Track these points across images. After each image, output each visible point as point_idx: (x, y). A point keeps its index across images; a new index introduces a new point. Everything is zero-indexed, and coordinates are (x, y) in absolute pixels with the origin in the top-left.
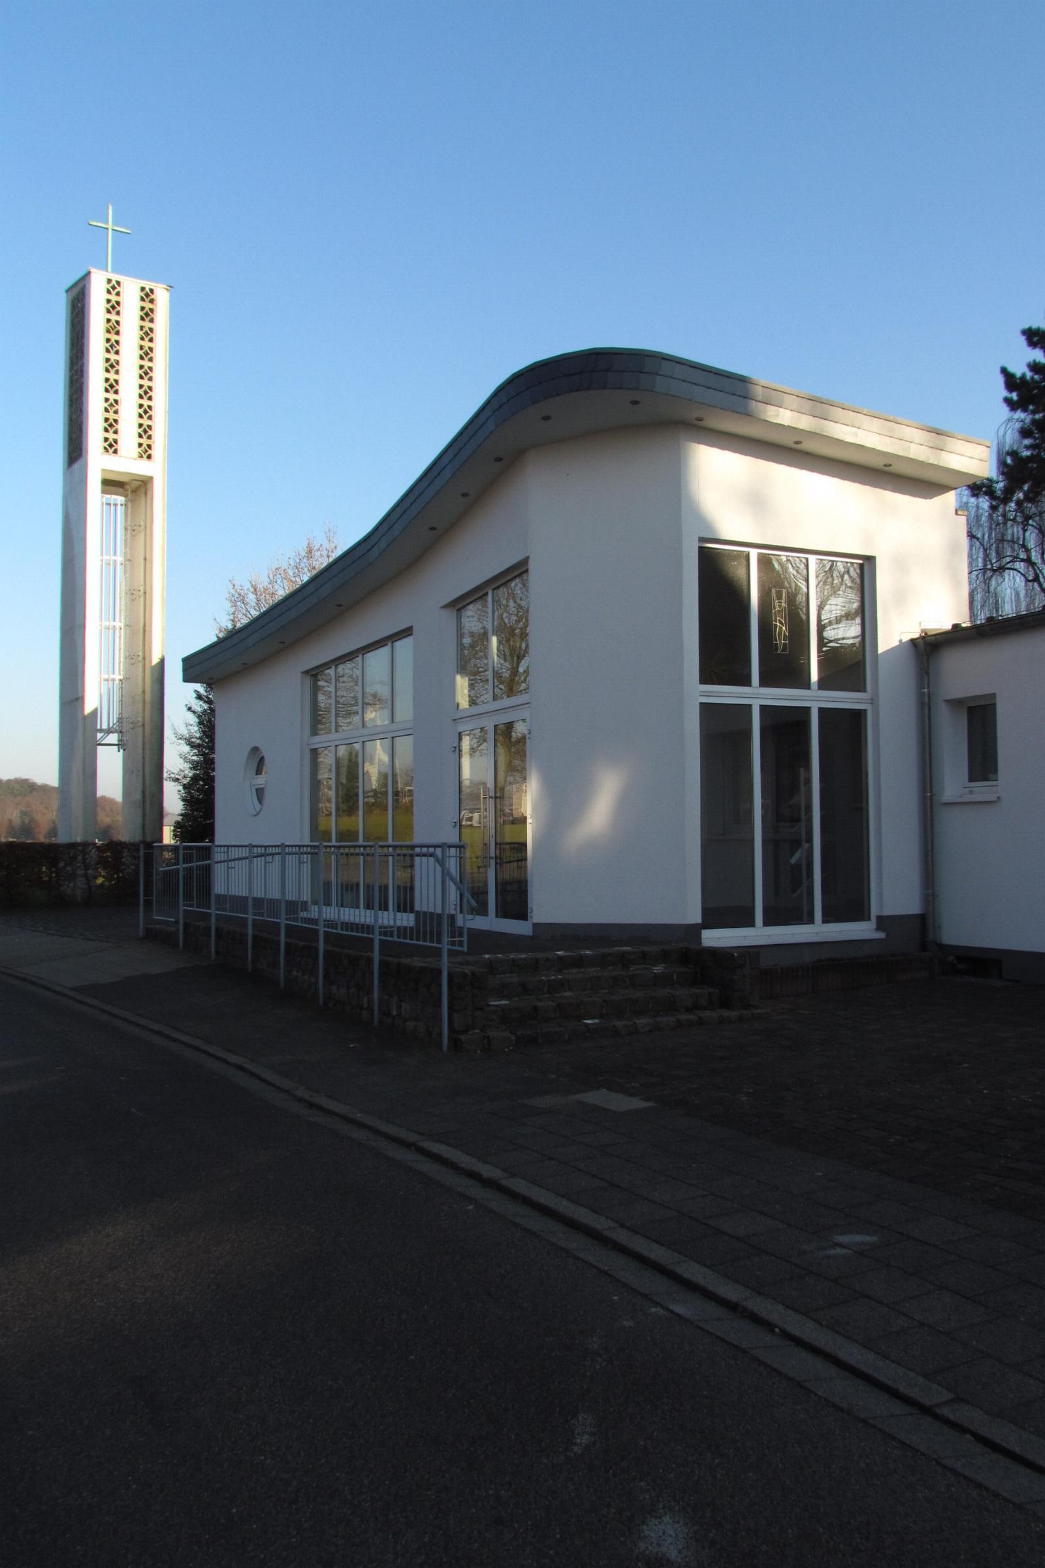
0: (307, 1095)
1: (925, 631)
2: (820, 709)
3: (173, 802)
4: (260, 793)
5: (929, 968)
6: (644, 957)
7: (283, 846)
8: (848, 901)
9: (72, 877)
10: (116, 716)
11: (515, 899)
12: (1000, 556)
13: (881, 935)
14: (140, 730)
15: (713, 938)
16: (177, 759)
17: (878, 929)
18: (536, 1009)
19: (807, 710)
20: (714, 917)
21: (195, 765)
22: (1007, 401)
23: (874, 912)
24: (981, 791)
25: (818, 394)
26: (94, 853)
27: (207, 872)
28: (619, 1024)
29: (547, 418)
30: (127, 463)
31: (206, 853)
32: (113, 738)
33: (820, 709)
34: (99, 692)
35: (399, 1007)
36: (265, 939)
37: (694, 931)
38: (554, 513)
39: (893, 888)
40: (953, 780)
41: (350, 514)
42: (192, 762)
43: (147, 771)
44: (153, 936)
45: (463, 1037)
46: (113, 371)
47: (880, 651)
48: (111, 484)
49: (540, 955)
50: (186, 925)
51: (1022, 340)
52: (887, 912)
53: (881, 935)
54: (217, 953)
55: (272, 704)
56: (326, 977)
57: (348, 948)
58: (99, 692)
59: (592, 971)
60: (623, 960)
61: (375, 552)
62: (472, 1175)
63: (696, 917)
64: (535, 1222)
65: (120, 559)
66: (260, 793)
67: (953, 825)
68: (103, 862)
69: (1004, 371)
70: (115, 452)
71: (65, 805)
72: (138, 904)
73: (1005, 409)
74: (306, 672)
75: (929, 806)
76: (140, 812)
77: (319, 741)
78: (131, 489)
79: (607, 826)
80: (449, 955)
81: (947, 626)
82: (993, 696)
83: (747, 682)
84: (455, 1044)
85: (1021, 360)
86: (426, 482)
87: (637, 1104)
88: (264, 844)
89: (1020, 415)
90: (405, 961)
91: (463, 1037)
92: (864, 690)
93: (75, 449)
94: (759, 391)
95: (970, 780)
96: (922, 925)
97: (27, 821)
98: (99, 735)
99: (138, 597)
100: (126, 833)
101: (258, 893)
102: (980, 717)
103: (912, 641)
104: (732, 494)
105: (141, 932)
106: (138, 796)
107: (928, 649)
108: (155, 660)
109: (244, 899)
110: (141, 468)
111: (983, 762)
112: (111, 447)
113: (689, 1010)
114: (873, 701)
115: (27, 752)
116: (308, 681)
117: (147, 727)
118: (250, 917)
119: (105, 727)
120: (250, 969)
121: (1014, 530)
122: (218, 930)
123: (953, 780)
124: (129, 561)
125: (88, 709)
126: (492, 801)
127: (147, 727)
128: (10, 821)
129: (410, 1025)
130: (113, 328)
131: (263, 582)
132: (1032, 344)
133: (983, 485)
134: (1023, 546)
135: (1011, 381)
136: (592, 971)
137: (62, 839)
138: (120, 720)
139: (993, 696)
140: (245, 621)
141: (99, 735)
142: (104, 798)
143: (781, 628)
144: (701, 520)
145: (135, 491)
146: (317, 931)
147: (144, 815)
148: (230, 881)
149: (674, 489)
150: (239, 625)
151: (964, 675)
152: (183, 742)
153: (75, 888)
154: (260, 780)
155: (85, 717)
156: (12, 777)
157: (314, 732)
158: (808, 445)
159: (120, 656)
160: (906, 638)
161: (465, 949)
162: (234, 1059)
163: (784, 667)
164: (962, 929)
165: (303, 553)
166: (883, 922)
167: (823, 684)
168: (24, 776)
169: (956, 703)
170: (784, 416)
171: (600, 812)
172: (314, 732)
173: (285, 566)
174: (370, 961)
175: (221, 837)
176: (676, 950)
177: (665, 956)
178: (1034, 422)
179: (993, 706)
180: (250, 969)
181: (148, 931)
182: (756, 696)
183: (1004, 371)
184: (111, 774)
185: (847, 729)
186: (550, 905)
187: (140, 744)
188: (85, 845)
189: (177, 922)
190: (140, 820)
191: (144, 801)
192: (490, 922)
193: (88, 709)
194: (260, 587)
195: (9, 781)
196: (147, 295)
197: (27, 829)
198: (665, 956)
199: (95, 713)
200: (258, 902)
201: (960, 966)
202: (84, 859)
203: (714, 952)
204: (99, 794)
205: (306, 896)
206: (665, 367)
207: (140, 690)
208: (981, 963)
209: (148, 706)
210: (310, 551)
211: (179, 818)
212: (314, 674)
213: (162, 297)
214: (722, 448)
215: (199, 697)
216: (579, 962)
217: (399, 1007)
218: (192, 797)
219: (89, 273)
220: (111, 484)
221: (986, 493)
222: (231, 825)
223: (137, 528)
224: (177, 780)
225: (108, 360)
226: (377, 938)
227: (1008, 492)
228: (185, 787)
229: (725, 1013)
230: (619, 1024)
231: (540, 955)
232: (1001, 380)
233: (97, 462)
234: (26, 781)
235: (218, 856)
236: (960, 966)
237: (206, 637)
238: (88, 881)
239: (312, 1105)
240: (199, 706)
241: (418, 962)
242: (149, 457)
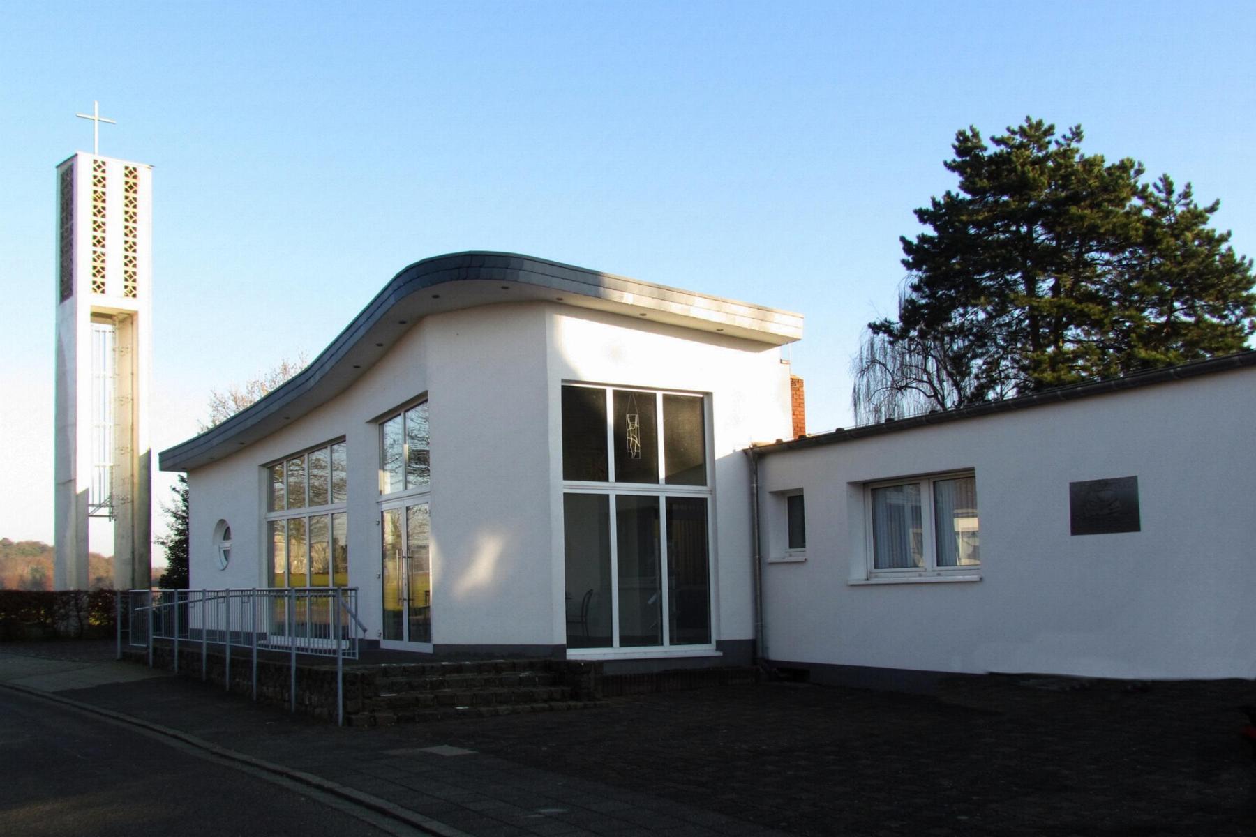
1: (755, 446)
2: (667, 498)
3: (160, 560)
4: (226, 553)
6: (514, 667)
7: (227, 591)
8: (693, 617)
9: (66, 617)
10: (107, 494)
11: (422, 630)
12: (904, 377)
13: (720, 654)
14: (129, 505)
15: (574, 654)
16: (163, 528)
17: (718, 649)
18: (417, 699)
19: (657, 499)
20: (573, 642)
21: (180, 532)
22: (904, 262)
23: (714, 638)
24: (797, 555)
25: (661, 283)
27: (184, 610)
28: (483, 709)
29: (436, 297)
30: (114, 300)
31: (184, 596)
32: (105, 511)
33: (667, 498)
35: (310, 699)
37: (561, 649)
38: (448, 358)
39: (730, 618)
40: (777, 546)
42: (178, 530)
45: (353, 717)
46: (100, 230)
47: (718, 456)
48: (98, 316)
49: (427, 665)
50: (155, 650)
51: (915, 218)
52: (723, 638)
53: (720, 654)
54: (180, 667)
55: (240, 483)
57: (274, 663)
58: (94, 474)
59: (470, 676)
60: (497, 669)
61: (312, 382)
62: (319, 787)
63: (562, 640)
64: (358, 811)
65: (109, 373)
66: (226, 553)
67: (776, 580)
68: (93, 605)
69: (903, 239)
70: (103, 292)
72: (115, 638)
73: (903, 269)
74: (264, 466)
75: (758, 564)
76: (129, 568)
77: (273, 516)
79: (494, 575)
80: (344, 664)
81: (772, 441)
82: (802, 490)
83: (606, 479)
84: (348, 721)
85: (917, 230)
86: (347, 336)
87: (466, 752)
89: (915, 272)
90: (315, 668)
91: (353, 717)
92: (705, 484)
93: (66, 289)
94: (606, 281)
95: (791, 546)
96: (753, 648)
97: (38, 576)
98: (91, 509)
99: (127, 403)
100: (119, 581)
101: (235, 627)
102: (795, 501)
103: (745, 451)
104: (588, 351)
105: (119, 655)
106: (128, 556)
107: (756, 457)
110: (128, 305)
111: (797, 537)
112: (99, 288)
113: (545, 701)
114: (713, 492)
115: (33, 523)
116: (265, 473)
117: (136, 503)
118: (205, 642)
119: (96, 502)
120: (204, 678)
121: (917, 359)
122: (180, 653)
123: (777, 546)
124: (118, 375)
126: (404, 561)
127: (136, 503)
128: (21, 576)
129: (318, 710)
130: (100, 197)
131: (242, 392)
133: (882, 325)
136: (470, 676)
138: (111, 497)
139: (802, 490)
140: (223, 419)
143: (634, 441)
144: (565, 366)
145: (122, 321)
146: (251, 650)
147: (134, 570)
148: (202, 617)
150: (218, 423)
151: (781, 474)
152: (169, 514)
153: (70, 625)
154: (227, 544)
155: (77, 496)
157: (271, 508)
158: (650, 316)
159: (110, 447)
160: (739, 449)
161: (357, 657)
162: (171, 732)
163: (636, 466)
164: (782, 649)
165: (278, 371)
166: (720, 645)
167: (669, 480)
168: (35, 539)
169: (779, 494)
170: (628, 298)
173: (262, 379)
174: (289, 668)
175: (194, 585)
176: (545, 665)
177: (531, 666)
178: (921, 280)
179: (802, 496)
180: (204, 678)
181: (124, 654)
182: (612, 488)
183: (903, 239)
184: (103, 538)
185: (690, 516)
186: (445, 632)
187: (130, 516)
189: (147, 648)
191: (133, 559)
192: (405, 645)
193: (80, 489)
194: (239, 395)
195: (19, 544)
196: (131, 172)
198: (531, 666)
199: (86, 492)
202: (76, 604)
203: (576, 665)
205: (264, 627)
206: (527, 265)
207: (129, 474)
210: (285, 368)
211: (165, 573)
212: (270, 466)
213: (145, 179)
214: (582, 318)
215: (183, 480)
216: (459, 669)
217: (310, 699)
218: (177, 557)
219: (76, 155)
220: (98, 316)
221: (885, 332)
222: (199, 579)
223: (125, 350)
224: (163, 543)
225: (95, 222)
227: (904, 334)
228: (170, 548)
229: (572, 703)
230: (483, 709)
231: (427, 665)
232: (901, 245)
234: (36, 544)
235: (192, 597)
237: (189, 432)
239: (222, 756)
240: (182, 487)
242: (134, 296)
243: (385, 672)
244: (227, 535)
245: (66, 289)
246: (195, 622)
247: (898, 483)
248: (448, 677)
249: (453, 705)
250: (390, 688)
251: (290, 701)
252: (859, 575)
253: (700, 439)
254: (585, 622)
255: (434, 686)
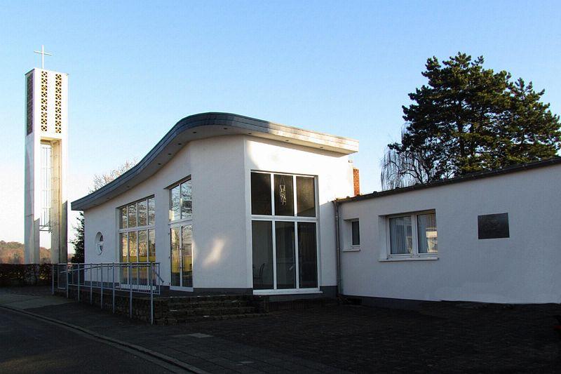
0: (98, 335)
3: (71, 250)
5: (335, 300)
6: (229, 298)
8: (309, 277)
11: (188, 281)
15: (256, 292)
16: (73, 236)
20: (256, 287)
21: (80, 238)
24: (356, 248)
26: (38, 267)
27: (82, 273)
30: (51, 134)
34: (42, 212)
36: (96, 293)
38: (200, 160)
39: (326, 277)
40: (347, 244)
41: (134, 154)
43: (61, 239)
44: (56, 294)
47: (320, 204)
48: (43, 141)
49: (191, 297)
50: (69, 290)
55: (107, 217)
56: (115, 304)
57: (123, 296)
58: (42, 212)
59: (210, 302)
60: (222, 299)
61: (139, 171)
65: (49, 167)
67: (346, 259)
68: (41, 271)
69: (403, 107)
71: (27, 251)
76: (58, 254)
78: (55, 143)
79: (220, 256)
82: (358, 219)
84: (155, 322)
88: (102, 266)
91: (158, 320)
93: (30, 129)
94: (271, 125)
96: (336, 289)
98: (41, 227)
99: (57, 180)
100: (53, 260)
101: (93, 280)
102: (355, 224)
105: (53, 293)
107: (338, 204)
108: (64, 202)
109: (89, 282)
110: (57, 136)
111: (356, 240)
112: (44, 129)
114: (318, 220)
115: (16, 235)
116: (119, 211)
118: (91, 287)
119: (43, 224)
121: (409, 161)
123: (347, 244)
125: (36, 219)
128: (9, 258)
130: (44, 88)
131: (108, 175)
132: (412, 98)
134: (413, 165)
135: (405, 110)
137: (24, 262)
141: (41, 227)
142: (42, 248)
143: (283, 197)
144: (252, 163)
147: (60, 255)
149: (242, 156)
151: (349, 212)
154: (101, 243)
155: (34, 222)
156: (10, 241)
157: (121, 228)
162: (76, 327)
163: (284, 209)
164: (350, 290)
170: (281, 133)
171: (216, 252)
172: (121, 228)
175: (87, 261)
176: (243, 298)
177: (237, 298)
178: (411, 125)
182: (273, 218)
183: (403, 107)
184: (46, 241)
185: (309, 231)
186: (199, 282)
187: (58, 231)
188: (34, 265)
190: (58, 257)
192: (181, 288)
193: (36, 219)
197: (147, 263)
198: (237, 298)
200: (94, 283)
201: (349, 302)
202: (34, 270)
203: (257, 296)
204: (41, 246)
206: (235, 118)
208: (357, 301)
209: (61, 218)
212: (121, 208)
215: (82, 215)
216: (205, 299)
220: (43, 141)
222: (89, 258)
223: (56, 156)
226: (131, 292)
227: (404, 149)
230: (216, 317)
231: (191, 297)
233: (38, 133)
235: (86, 267)
236: (349, 302)
238: (36, 277)
239: (99, 338)
241: (145, 299)
243: (172, 300)
244: (101, 239)
245: (30, 129)
246: (87, 278)
247: (401, 216)
248: (200, 303)
249: (202, 315)
250: (174, 307)
251: (129, 313)
252: (383, 257)
253: (311, 194)
254: (261, 278)
255: (194, 306)
